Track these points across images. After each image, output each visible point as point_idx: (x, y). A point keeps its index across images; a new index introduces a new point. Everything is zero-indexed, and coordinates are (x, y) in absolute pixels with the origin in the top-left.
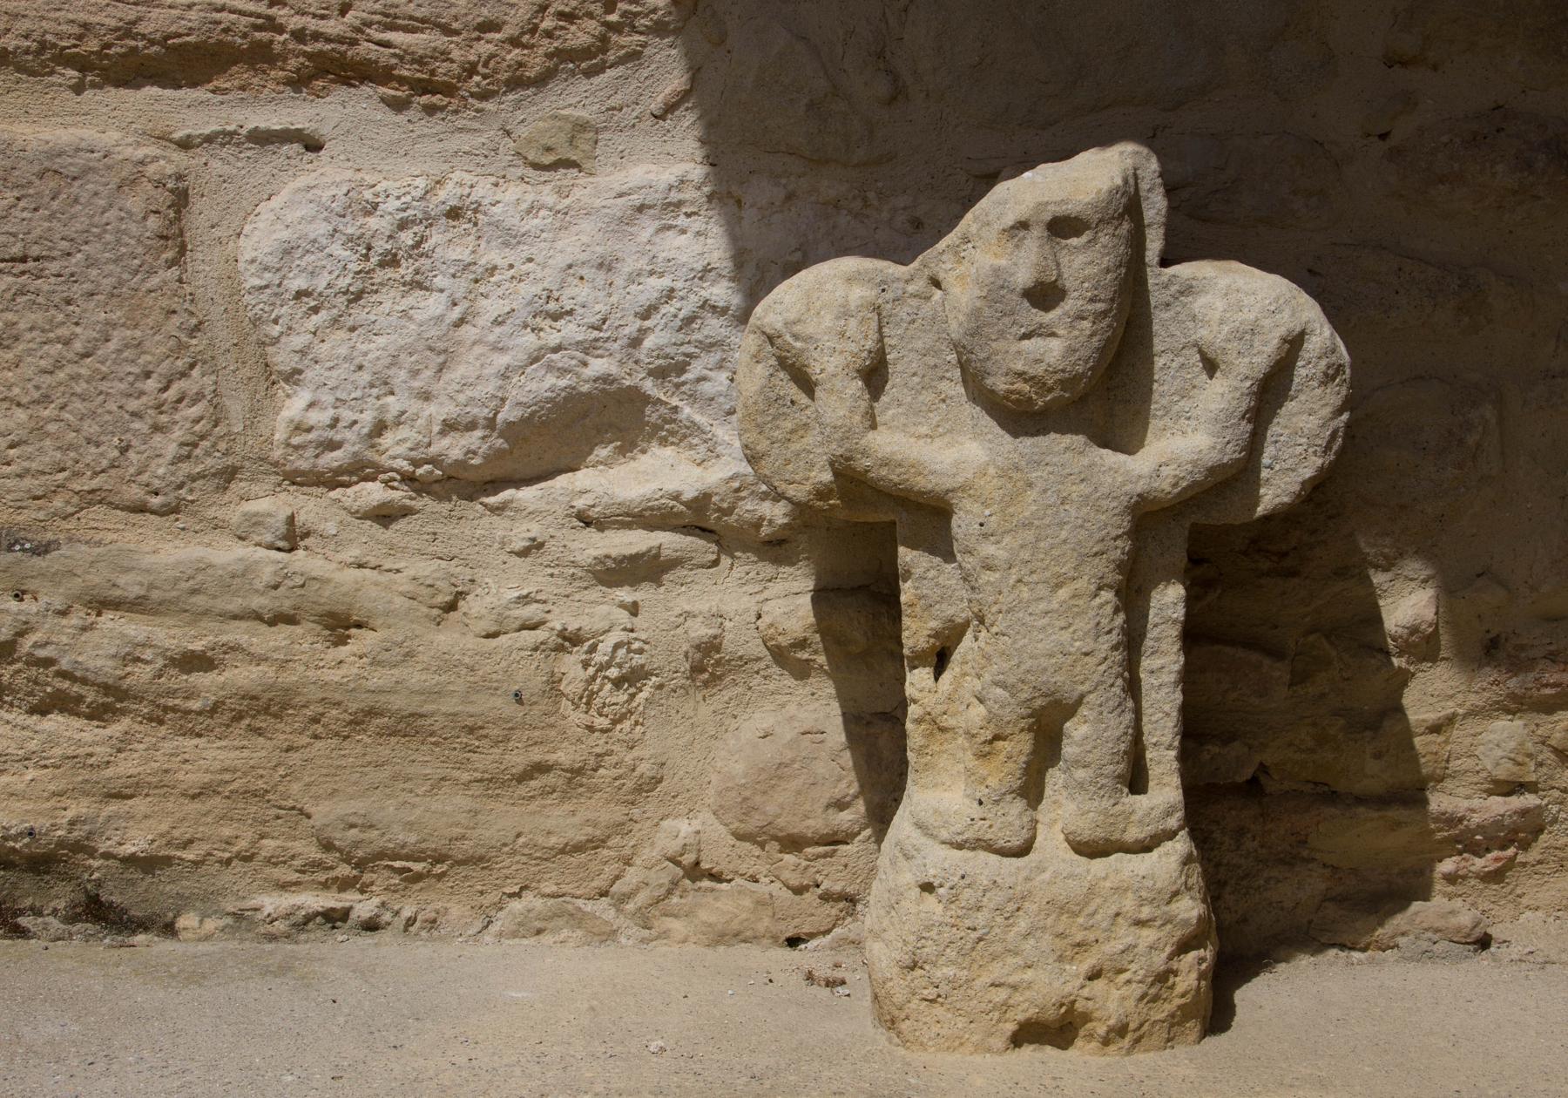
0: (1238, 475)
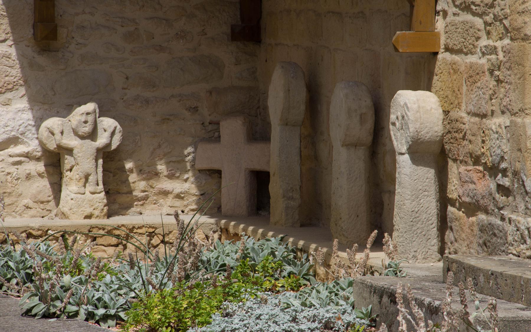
0: (109, 145)
